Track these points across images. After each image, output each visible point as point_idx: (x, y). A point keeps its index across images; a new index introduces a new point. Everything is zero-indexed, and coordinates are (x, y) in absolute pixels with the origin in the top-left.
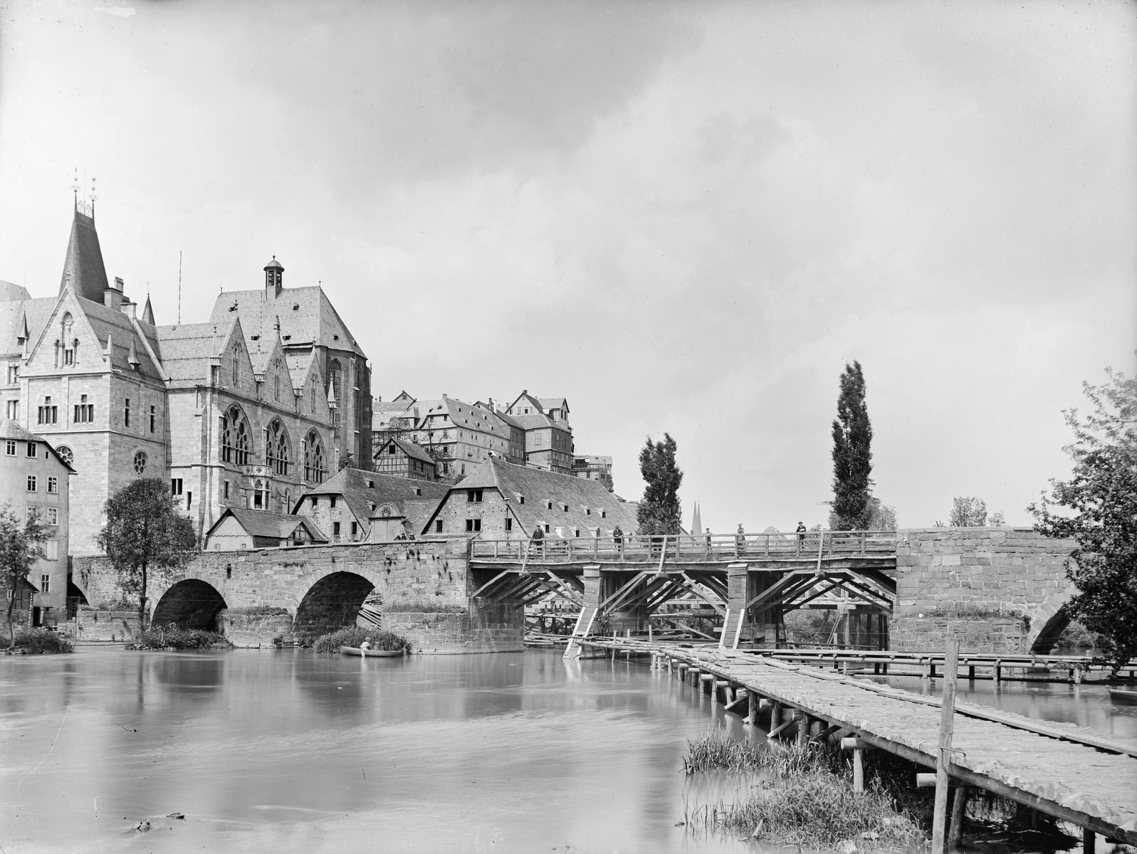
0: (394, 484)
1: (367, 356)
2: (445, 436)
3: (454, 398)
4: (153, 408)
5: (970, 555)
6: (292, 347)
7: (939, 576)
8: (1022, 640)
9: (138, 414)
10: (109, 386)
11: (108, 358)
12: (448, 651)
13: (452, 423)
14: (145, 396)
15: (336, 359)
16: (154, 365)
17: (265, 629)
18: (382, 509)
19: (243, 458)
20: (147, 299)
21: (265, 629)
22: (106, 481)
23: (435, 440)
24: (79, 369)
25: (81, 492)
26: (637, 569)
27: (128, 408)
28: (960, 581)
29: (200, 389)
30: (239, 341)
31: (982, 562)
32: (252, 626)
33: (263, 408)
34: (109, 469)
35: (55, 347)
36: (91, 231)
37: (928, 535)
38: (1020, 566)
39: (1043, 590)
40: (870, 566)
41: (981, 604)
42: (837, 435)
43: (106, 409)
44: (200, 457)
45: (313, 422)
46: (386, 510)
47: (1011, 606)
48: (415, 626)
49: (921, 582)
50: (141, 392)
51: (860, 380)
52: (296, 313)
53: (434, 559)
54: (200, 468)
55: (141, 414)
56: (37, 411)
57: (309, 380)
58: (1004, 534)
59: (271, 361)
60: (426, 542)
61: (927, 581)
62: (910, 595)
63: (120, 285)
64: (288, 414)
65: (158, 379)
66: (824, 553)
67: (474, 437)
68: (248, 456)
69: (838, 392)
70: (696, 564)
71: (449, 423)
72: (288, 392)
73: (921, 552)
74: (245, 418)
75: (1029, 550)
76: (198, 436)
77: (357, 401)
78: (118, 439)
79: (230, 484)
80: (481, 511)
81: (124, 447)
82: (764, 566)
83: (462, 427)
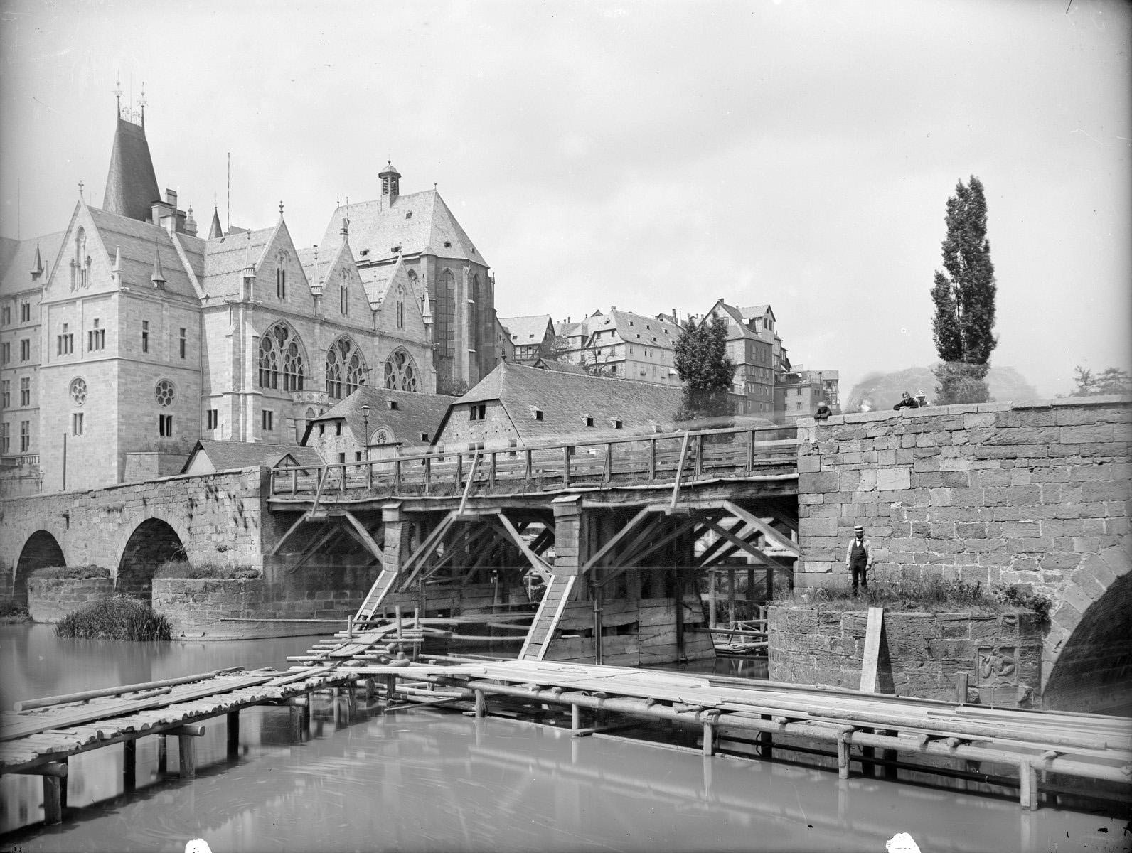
0: (432, 404)
1: (489, 264)
2: (613, 354)
3: (626, 310)
4: (183, 330)
5: (927, 466)
6: (408, 258)
7: (873, 511)
8: (1023, 654)
9: (161, 337)
10: (117, 307)
11: (116, 275)
12: (223, 635)
13: (620, 339)
14: (171, 317)
15: (447, 270)
16: (190, 282)
17: (67, 598)
18: (377, 434)
19: (297, 382)
20: (214, 213)
21: (67, 598)
22: (115, 416)
23: (601, 359)
24: (93, 290)
25: (95, 428)
26: (444, 508)
27: (146, 331)
28: (910, 522)
29: (232, 305)
30: (285, 248)
31: (952, 481)
32: (51, 594)
33: (321, 324)
34: (119, 401)
35: (70, 268)
36: (139, 140)
37: (850, 428)
38: (1025, 487)
39: (1077, 542)
40: (762, 494)
41: (951, 570)
42: (940, 296)
43: (115, 332)
44: (231, 384)
45: (399, 340)
46: (382, 436)
47: (1009, 576)
48: (175, 599)
49: (840, 524)
50: (164, 312)
51: (981, 205)
52: (409, 221)
53: (230, 498)
54: (230, 396)
55: (165, 337)
56: (56, 340)
57: (393, 291)
58: (993, 417)
59: (334, 270)
60: (223, 474)
61: (852, 522)
62: (822, 551)
63: (172, 198)
64: (361, 331)
65: (193, 298)
66: (688, 471)
67: (648, 354)
68: (304, 380)
69: (941, 232)
70: (513, 498)
71: (617, 339)
72: (362, 307)
73: (837, 464)
74: (297, 337)
75: (1043, 451)
76: (229, 359)
77: (472, 315)
78: (131, 366)
79: (275, 414)
80: (483, 432)
81: (140, 376)
82: (604, 499)
83: (632, 343)
